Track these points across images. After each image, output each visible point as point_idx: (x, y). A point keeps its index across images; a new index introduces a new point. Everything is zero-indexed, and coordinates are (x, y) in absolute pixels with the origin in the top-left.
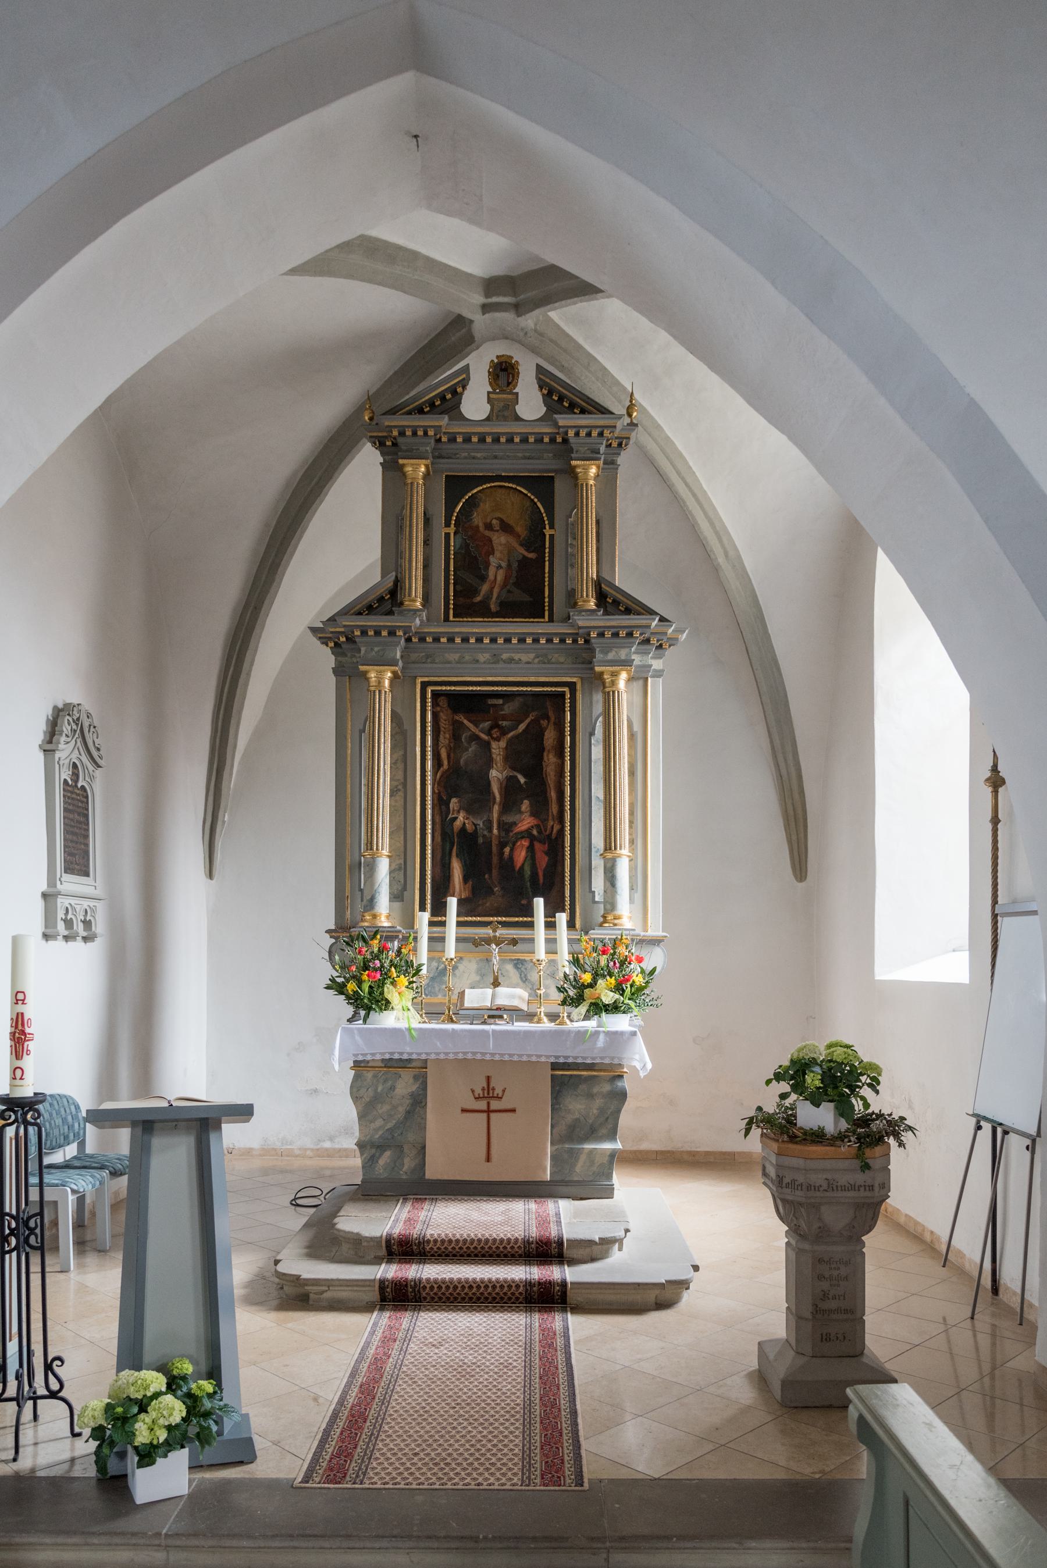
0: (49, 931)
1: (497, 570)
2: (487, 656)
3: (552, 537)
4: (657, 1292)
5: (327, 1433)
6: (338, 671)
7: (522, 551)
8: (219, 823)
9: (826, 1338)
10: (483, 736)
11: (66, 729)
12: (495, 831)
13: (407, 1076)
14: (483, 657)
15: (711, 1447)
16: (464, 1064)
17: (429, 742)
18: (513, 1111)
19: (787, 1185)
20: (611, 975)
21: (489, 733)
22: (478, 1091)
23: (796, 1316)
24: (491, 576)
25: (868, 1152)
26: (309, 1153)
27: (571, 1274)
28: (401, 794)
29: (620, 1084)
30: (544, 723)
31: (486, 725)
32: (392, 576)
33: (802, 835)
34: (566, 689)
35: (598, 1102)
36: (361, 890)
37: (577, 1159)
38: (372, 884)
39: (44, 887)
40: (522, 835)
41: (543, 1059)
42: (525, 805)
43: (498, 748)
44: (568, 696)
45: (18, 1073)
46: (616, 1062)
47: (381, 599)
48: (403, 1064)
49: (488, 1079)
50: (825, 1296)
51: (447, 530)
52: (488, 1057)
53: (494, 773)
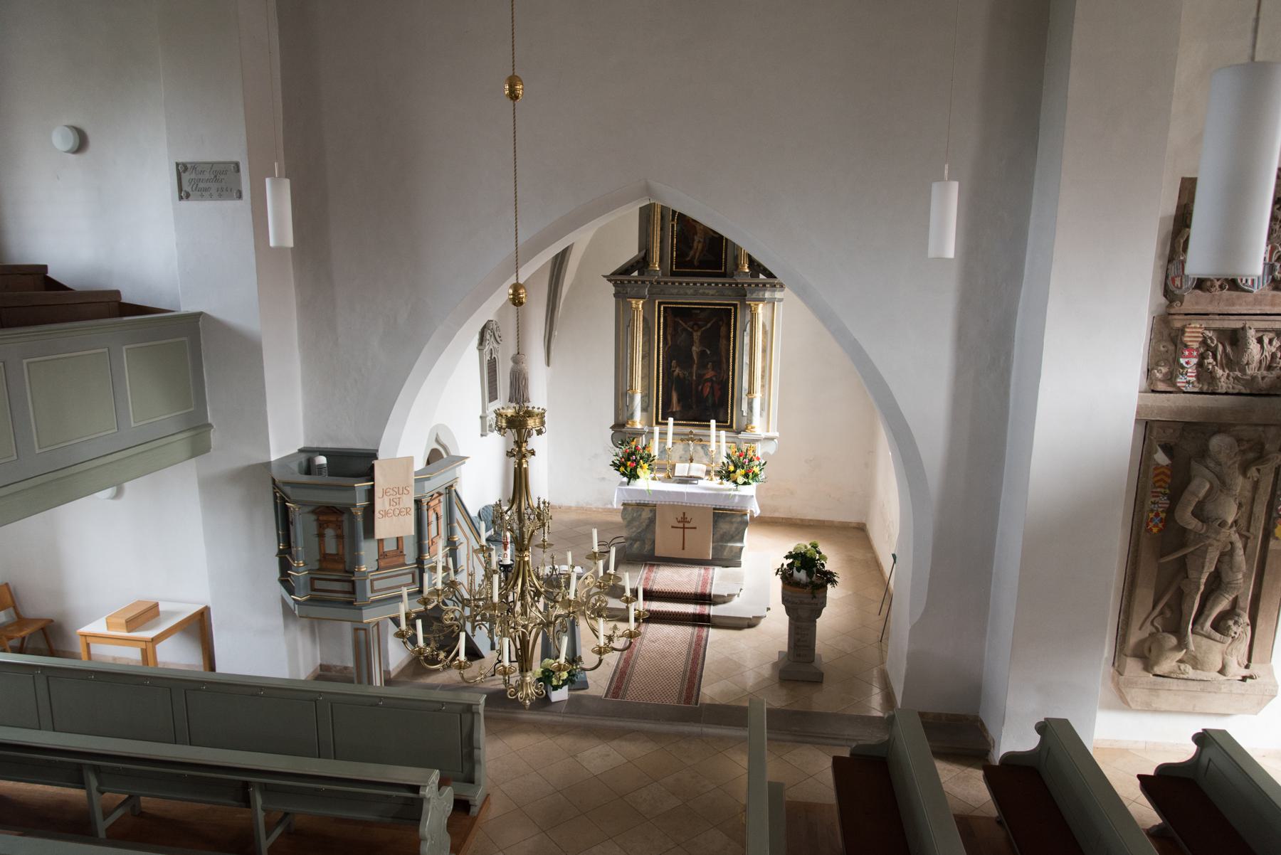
0: (484, 433)
2: (692, 291)
5: (612, 679)
6: (615, 295)
8: (553, 336)
9: (799, 655)
10: (689, 329)
11: (488, 337)
12: (694, 378)
13: (647, 509)
14: (690, 292)
16: (673, 507)
17: (661, 333)
18: (695, 528)
20: (743, 468)
21: (692, 328)
22: (679, 519)
23: (789, 647)
24: (695, 247)
26: (600, 510)
27: (713, 611)
28: (647, 358)
29: (745, 518)
30: (721, 323)
31: (691, 323)
32: (644, 251)
35: (735, 525)
37: (725, 549)
38: (632, 407)
39: (480, 413)
40: (707, 381)
41: (710, 506)
42: (710, 365)
43: (696, 336)
44: (733, 311)
46: (743, 509)
47: (638, 262)
48: (645, 505)
49: (684, 513)
50: (799, 640)
51: (673, 223)
52: (684, 504)
53: (694, 348)
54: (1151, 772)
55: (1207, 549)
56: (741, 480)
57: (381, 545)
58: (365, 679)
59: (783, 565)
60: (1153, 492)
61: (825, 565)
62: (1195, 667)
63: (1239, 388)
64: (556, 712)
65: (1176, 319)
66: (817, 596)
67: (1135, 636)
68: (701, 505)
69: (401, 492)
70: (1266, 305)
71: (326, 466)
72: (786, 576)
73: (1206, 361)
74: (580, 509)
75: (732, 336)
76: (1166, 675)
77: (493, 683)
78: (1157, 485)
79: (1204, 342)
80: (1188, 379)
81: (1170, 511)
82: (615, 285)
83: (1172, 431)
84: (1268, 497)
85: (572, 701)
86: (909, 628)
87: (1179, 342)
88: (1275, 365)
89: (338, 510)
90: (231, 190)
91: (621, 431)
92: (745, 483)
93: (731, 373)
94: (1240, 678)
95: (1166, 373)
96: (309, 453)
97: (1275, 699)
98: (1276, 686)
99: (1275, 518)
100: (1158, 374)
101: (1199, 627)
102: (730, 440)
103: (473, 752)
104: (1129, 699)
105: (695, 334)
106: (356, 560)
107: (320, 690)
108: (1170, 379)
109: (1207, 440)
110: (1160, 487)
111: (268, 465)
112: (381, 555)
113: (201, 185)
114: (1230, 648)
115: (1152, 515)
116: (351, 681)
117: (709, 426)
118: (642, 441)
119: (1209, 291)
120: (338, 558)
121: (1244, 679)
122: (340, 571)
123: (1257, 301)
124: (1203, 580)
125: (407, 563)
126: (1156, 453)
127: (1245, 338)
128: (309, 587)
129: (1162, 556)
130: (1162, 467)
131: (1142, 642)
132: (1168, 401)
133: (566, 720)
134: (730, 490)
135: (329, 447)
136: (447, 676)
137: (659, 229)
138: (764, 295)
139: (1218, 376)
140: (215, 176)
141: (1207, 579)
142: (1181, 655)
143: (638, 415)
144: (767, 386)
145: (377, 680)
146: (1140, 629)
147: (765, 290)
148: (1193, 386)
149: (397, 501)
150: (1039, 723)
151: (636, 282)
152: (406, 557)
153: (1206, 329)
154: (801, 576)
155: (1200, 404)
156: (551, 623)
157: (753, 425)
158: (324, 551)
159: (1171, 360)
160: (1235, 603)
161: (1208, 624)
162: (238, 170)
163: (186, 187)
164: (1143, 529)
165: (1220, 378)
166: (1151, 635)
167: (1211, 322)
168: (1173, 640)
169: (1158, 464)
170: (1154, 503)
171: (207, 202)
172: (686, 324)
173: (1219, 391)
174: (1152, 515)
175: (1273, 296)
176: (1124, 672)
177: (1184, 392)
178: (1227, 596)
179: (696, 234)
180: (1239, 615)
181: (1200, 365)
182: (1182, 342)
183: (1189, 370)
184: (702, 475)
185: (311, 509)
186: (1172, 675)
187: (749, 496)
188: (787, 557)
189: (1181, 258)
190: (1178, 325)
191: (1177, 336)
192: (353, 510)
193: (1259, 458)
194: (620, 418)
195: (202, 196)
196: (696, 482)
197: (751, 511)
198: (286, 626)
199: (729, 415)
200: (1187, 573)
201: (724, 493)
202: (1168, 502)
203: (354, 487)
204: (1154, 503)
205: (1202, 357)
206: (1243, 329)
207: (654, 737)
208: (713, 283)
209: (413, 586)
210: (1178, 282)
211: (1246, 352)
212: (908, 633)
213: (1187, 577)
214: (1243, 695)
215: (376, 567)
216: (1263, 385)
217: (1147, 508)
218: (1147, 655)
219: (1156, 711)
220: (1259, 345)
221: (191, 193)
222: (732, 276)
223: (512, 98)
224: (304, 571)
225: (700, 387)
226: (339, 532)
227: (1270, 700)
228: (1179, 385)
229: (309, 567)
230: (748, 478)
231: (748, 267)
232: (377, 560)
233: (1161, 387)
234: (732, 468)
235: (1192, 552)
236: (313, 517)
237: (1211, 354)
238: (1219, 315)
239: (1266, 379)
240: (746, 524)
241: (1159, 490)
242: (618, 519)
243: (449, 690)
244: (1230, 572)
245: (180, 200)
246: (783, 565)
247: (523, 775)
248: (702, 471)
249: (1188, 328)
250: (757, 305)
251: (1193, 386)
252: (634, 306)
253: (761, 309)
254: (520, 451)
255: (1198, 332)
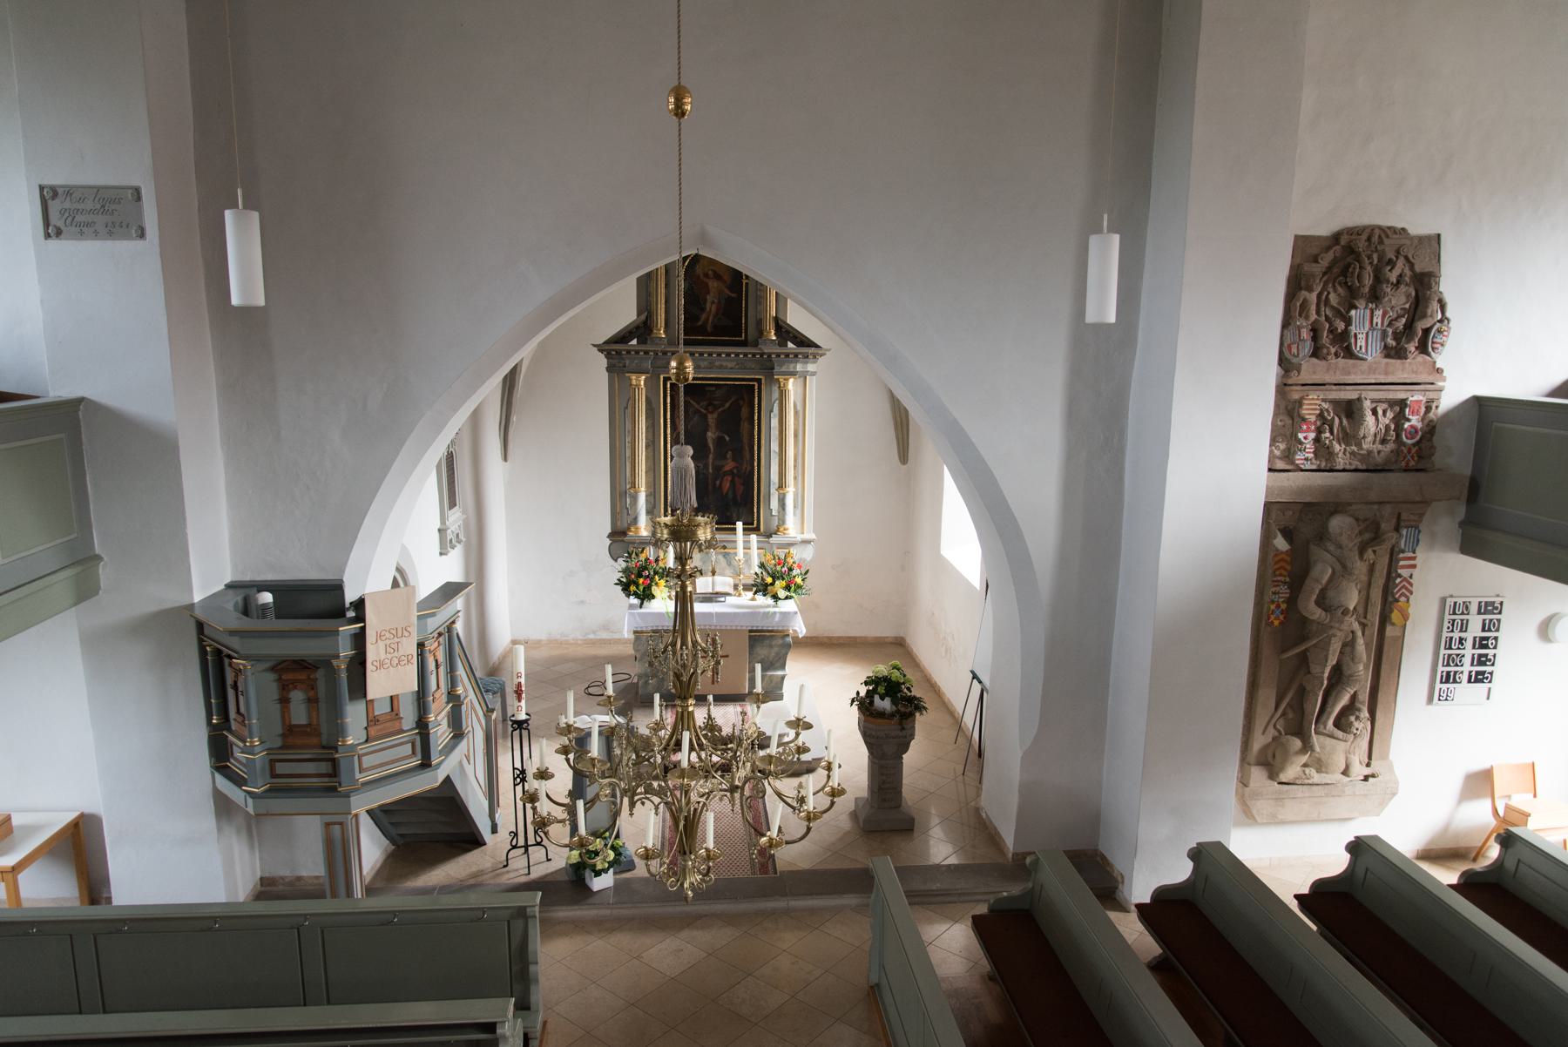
0: (443, 551)
1: (711, 305)
2: (706, 363)
3: (747, 284)
4: (807, 765)
6: (609, 369)
7: (728, 292)
10: (702, 410)
12: (711, 471)
15: (830, 853)
17: (669, 417)
19: (869, 736)
20: (783, 579)
24: (708, 309)
25: (904, 721)
26: (579, 642)
28: (652, 448)
30: (741, 402)
31: (705, 403)
33: (906, 438)
34: (755, 383)
36: (627, 509)
38: (636, 509)
39: (438, 525)
40: (726, 474)
41: (744, 628)
42: (729, 455)
43: (712, 419)
44: (756, 387)
45: (520, 708)
46: (785, 628)
47: (638, 328)
50: (884, 782)
53: (709, 434)
54: (1305, 890)
55: (1330, 640)
56: (782, 594)
57: (370, 707)
58: (342, 890)
59: (858, 693)
60: (1274, 581)
61: (912, 689)
62: (1319, 771)
63: (1356, 464)
64: (602, 904)
65: (1292, 390)
66: (905, 726)
67: (1259, 741)
68: (734, 628)
69: (400, 635)
70: (1380, 374)
71: (272, 605)
72: (865, 705)
73: (1323, 435)
74: (552, 642)
75: (756, 418)
76: (1291, 782)
77: (507, 876)
78: (1277, 573)
79: (1321, 416)
80: (1307, 455)
81: (1292, 601)
82: (608, 355)
83: (1291, 513)
84: (1383, 581)
85: (618, 887)
86: (1021, 755)
87: (1296, 414)
88: (1389, 438)
89: (310, 664)
90: (127, 227)
91: (623, 541)
92: (787, 598)
93: (756, 464)
94: (1362, 778)
95: (1284, 450)
96: (243, 590)
97: (1396, 797)
98: (1397, 783)
99: (1391, 603)
100: (1276, 451)
101: (1322, 727)
102: (762, 545)
103: (528, 968)
104: (1254, 812)
105: (710, 416)
106: (339, 730)
107: (306, 912)
108: (1287, 457)
109: (1327, 519)
110: (1281, 575)
111: (191, 607)
112: (371, 721)
113: (79, 218)
114: (1353, 747)
115: (1273, 607)
116: (318, 894)
117: (735, 529)
118: (650, 552)
119: (1325, 359)
120: (310, 730)
121: (1366, 778)
122: (314, 747)
123: (1371, 370)
124: (1326, 675)
125: (405, 729)
126: (1275, 538)
127: (1361, 409)
128: (268, 773)
129: (1284, 651)
130: (1282, 552)
131: (1265, 748)
132: (1288, 480)
133: (615, 912)
134: (768, 606)
135: (269, 579)
136: (444, 874)
137: (663, 286)
138: (795, 368)
139: (1336, 451)
140: (103, 206)
141: (1329, 674)
142: (1304, 758)
143: (643, 520)
144: (800, 478)
145: (358, 892)
146: (1264, 733)
147: (796, 362)
148: (1311, 464)
149: (395, 646)
150: (1191, 850)
151: (637, 352)
152: (403, 721)
153: (1323, 400)
154: (885, 704)
155: (1319, 482)
156: (737, 787)
157: (786, 526)
158: (290, 721)
159: (1288, 434)
160: (1354, 697)
161: (1331, 722)
162: (139, 198)
163: (55, 219)
164: (1264, 622)
165: (1338, 454)
166: (1274, 739)
167: (1327, 392)
168: (1297, 743)
169: (1277, 550)
170: (1274, 593)
171: (89, 242)
172: (699, 404)
173: (1337, 468)
174: (1273, 607)
175: (1387, 364)
176: (1248, 782)
177: (1302, 470)
178: (1349, 689)
179: (709, 293)
180: (1359, 710)
181: (1317, 440)
182: (1299, 415)
183: (1308, 446)
184: (731, 591)
185: (268, 665)
186: (1297, 782)
187: (791, 613)
188: (866, 683)
189: (1298, 323)
190: (1296, 396)
191: (1294, 408)
192: (335, 662)
193: (1375, 538)
194: (619, 523)
195: (82, 233)
196: (723, 599)
197: (795, 631)
198: (219, 829)
199: (756, 514)
200: (1308, 667)
201: (762, 610)
202: (1288, 591)
203: (338, 630)
204: (1274, 593)
205: (1319, 431)
206: (1359, 399)
207: (730, 920)
208: (733, 353)
209: (415, 759)
210: (1294, 350)
211: (1362, 424)
212: (1019, 759)
213: (1309, 673)
214: (1366, 795)
215: (365, 738)
216: (1379, 459)
217: (1267, 599)
218: (1272, 762)
219: (1283, 823)
220: (1374, 417)
221: (62, 228)
222: (756, 345)
223: (676, 115)
224: (261, 752)
225: (718, 482)
226: (311, 694)
227: (1392, 798)
228: (1297, 462)
229: (268, 745)
230: (789, 591)
231: (775, 334)
232: (366, 728)
233: (1280, 465)
234: (769, 580)
235: (1314, 645)
236: (271, 676)
237: (1328, 428)
238: (1335, 385)
239: (1383, 453)
240: (789, 646)
241: (1279, 578)
242: (631, 651)
243: (450, 893)
244: (1351, 664)
245: (46, 239)
246: (858, 693)
247: (580, 990)
248: (729, 585)
249: (1306, 399)
250: (787, 380)
251: (1311, 464)
252: (634, 382)
253: (792, 385)
254: (683, 570)
255: (1316, 404)
